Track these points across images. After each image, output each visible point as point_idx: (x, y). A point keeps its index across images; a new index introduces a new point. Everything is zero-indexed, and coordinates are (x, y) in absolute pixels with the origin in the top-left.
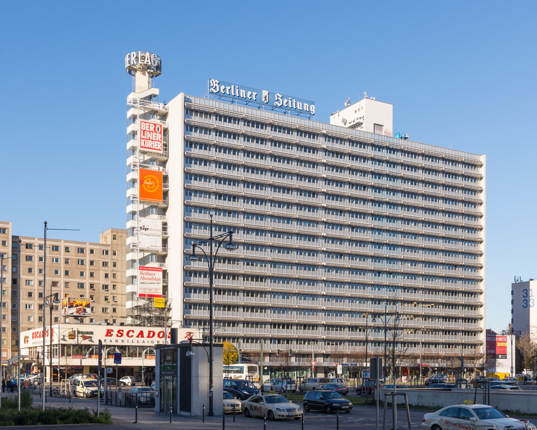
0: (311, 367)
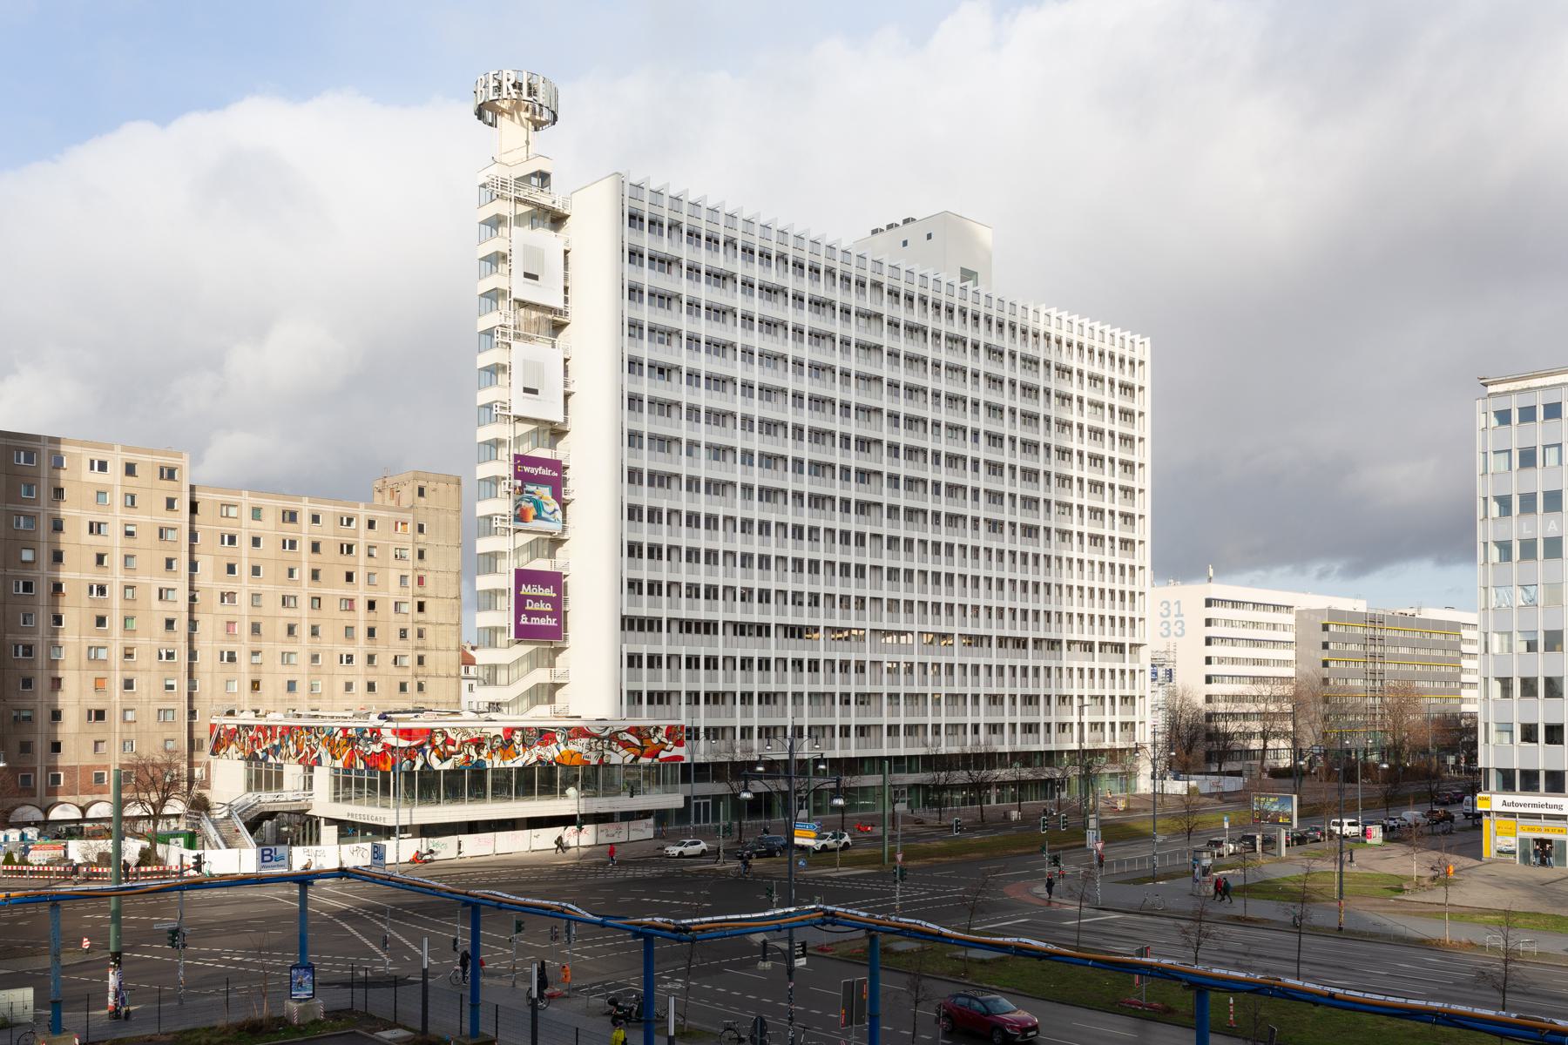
0: (833, 695)
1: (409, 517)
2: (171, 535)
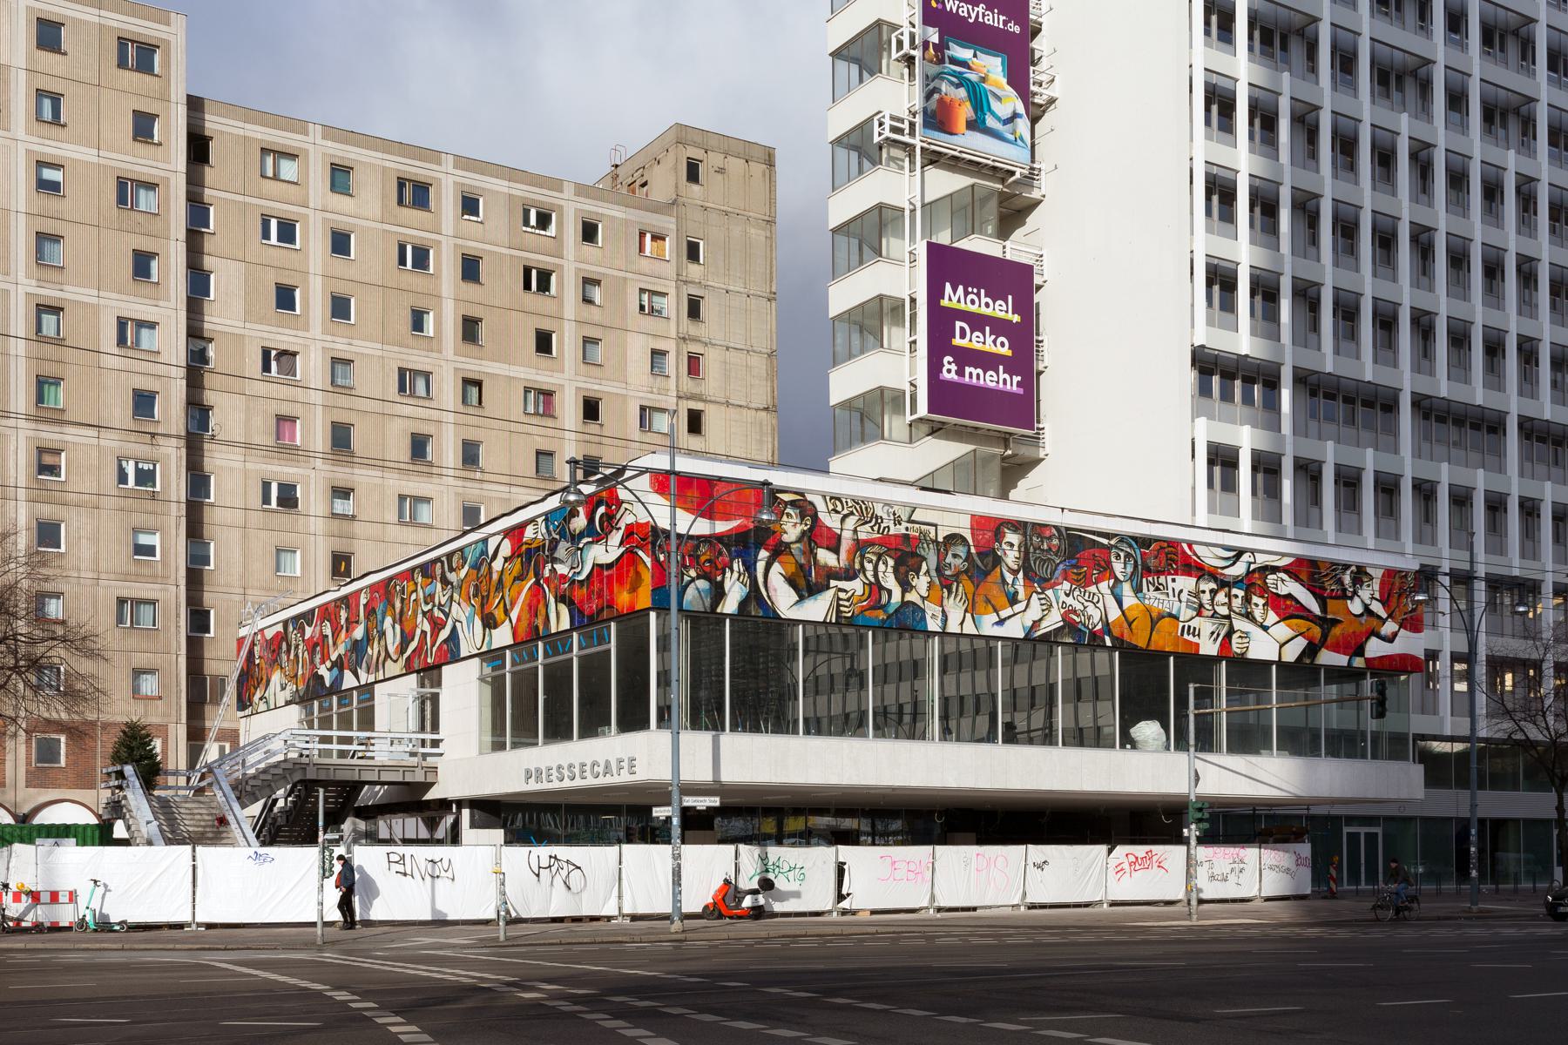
1: (667, 223)
2: (146, 200)
